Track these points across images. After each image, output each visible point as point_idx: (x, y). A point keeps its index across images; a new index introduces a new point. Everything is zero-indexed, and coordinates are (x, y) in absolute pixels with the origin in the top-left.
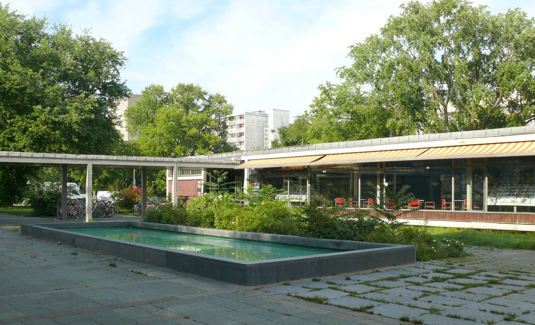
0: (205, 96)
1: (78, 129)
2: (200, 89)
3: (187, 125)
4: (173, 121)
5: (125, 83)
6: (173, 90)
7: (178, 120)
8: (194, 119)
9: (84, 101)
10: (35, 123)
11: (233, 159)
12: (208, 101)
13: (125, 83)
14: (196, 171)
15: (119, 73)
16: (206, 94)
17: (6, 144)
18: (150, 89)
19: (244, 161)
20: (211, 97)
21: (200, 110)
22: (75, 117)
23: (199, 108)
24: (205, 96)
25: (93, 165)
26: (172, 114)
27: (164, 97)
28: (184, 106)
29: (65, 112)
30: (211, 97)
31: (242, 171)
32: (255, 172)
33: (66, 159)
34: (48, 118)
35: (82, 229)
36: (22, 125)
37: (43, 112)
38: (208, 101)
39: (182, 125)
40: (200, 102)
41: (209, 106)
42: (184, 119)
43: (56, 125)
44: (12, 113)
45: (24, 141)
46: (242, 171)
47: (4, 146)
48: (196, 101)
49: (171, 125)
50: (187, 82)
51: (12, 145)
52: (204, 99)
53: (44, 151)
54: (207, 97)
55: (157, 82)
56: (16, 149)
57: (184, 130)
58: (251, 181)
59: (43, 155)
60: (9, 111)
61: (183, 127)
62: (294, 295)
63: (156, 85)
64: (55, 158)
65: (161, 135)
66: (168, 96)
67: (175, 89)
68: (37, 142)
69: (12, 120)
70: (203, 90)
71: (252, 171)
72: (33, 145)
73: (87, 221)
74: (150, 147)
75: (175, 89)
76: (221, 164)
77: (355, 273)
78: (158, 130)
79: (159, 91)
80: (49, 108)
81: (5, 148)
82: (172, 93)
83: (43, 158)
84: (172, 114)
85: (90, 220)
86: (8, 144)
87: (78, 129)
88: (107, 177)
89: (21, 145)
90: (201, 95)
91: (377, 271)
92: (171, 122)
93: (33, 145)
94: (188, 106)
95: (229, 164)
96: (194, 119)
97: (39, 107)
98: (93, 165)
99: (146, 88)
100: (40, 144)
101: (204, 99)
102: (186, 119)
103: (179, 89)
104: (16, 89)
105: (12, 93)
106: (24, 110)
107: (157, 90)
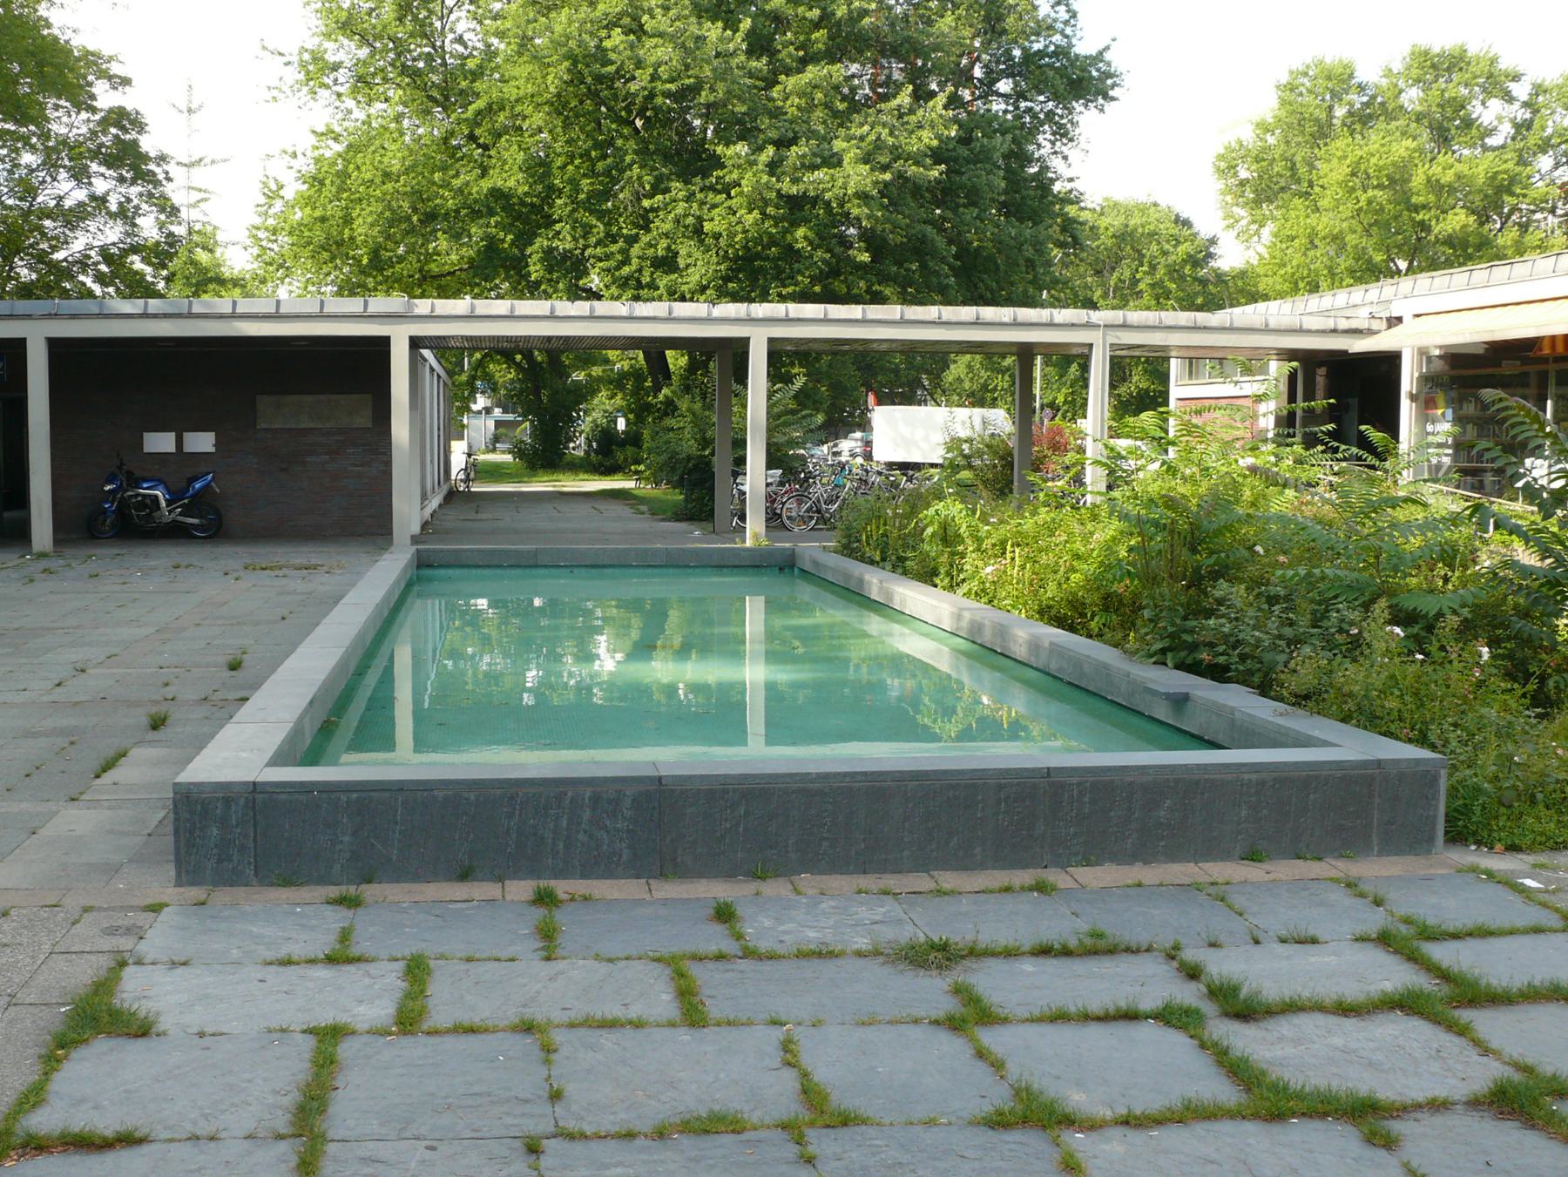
0: (1512, 86)
1: (869, 217)
2: (1493, 61)
3: (1432, 198)
4: (1380, 186)
5: (1107, 48)
6: (1388, 73)
7: (1397, 180)
8: (1459, 177)
9: (913, 118)
10: (729, 203)
11: (1364, 312)
12: (1526, 105)
13: (1107, 48)
14: (1251, 363)
15: (1074, 15)
16: (1516, 78)
17: (646, 279)
18: (1306, 74)
19: (1399, 320)
20: (1539, 89)
21: (1489, 141)
22: (855, 176)
23: (1490, 132)
24: (1512, 86)
25: (771, 340)
26: (1373, 160)
27: (1358, 100)
28: (1431, 127)
29: (834, 161)
30: (1539, 89)
31: (1391, 361)
32: (1439, 366)
33: (670, 319)
34: (768, 187)
35: (607, 571)
36: (686, 216)
37: (753, 163)
38: (1526, 105)
39: (1414, 200)
40: (1489, 112)
41: (1528, 125)
42: (1418, 180)
43: (797, 207)
44: (662, 175)
45: (699, 266)
46: (1391, 361)
47: (640, 286)
48: (1475, 109)
49: (1369, 202)
50: (1440, 41)
51: (663, 281)
52: (1509, 98)
53: (764, 298)
54: (1521, 91)
55: (1333, 53)
56: (676, 295)
57: (1419, 217)
58: (1425, 402)
59: (592, 309)
60: (654, 169)
61: (1416, 209)
62: (863, 943)
63: (1328, 60)
64: (631, 318)
65: (1337, 239)
66: (1374, 97)
67: (1397, 67)
68: (739, 270)
69: (659, 197)
70: (1504, 64)
71: (1429, 359)
72: (726, 279)
73: (748, 544)
74: (1296, 283)
75: (1397, 67)
76: (1301, 331)
77: (864, 881)
78: (1324, 223)
79: (1339, 80)
80: (771, 150)
81: (644, 293)
82: (1384, 82)
83: (592, 317)
84: (1373, 160)
85: (756, 536)
86: (653, 280)
87: (869, 217)
88: (1147, 391)
89: (694, 277)
90: (1496, 83)
91: (1041, 888)
92: (1370, 193)
93: (726, 279)
94: (1448, 126)
95: (1334, 331)
96: (1459, 177)
97: (742, 148)
98: (771, 340)
99: (1291, 72)
100: (749, 274)
101: (1509, 98)
102: (1429, 181)
103: (1408, 68)
104: (667, 94)
105: (656, 109)
106: (694, 162)
107: (1329, 78)
